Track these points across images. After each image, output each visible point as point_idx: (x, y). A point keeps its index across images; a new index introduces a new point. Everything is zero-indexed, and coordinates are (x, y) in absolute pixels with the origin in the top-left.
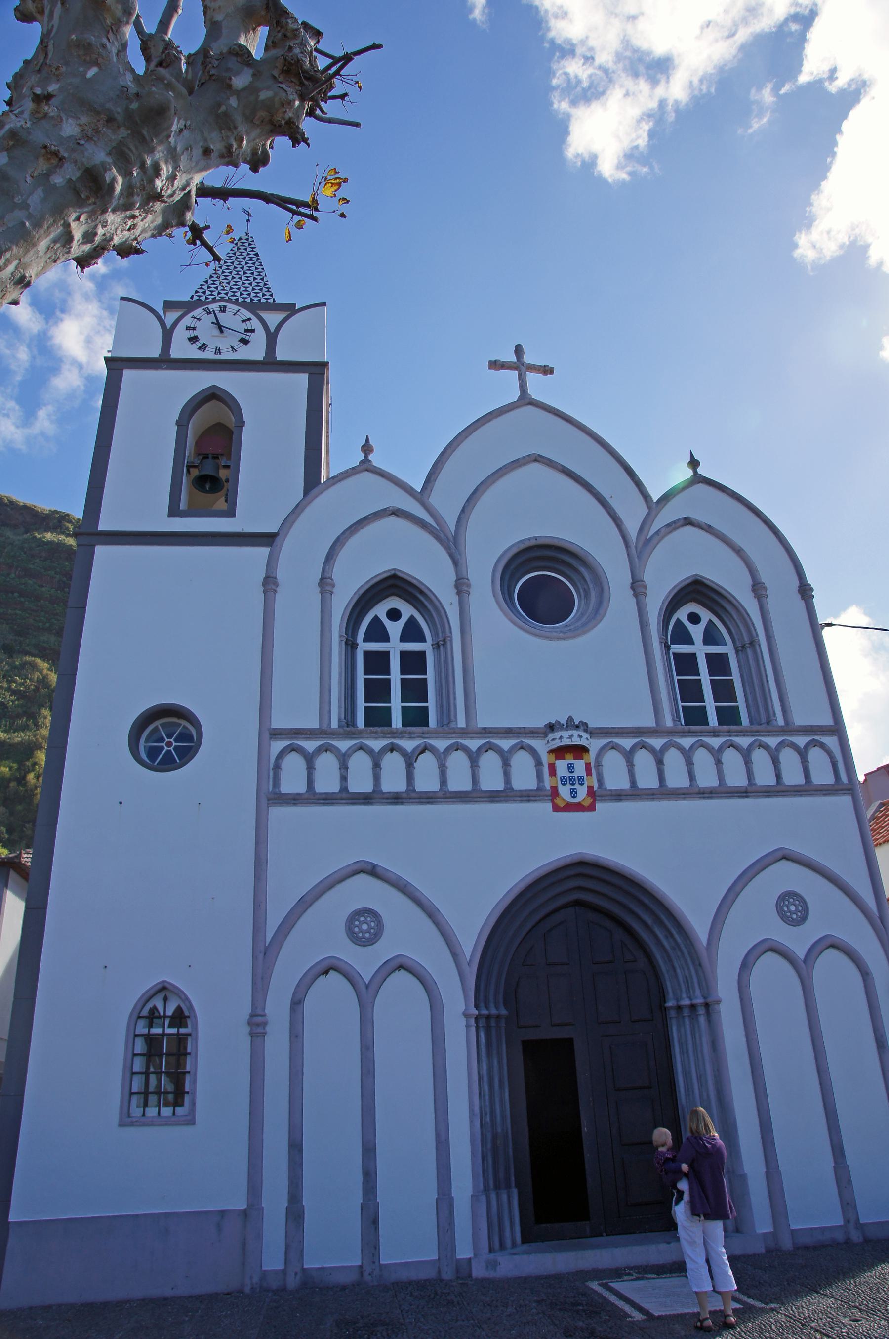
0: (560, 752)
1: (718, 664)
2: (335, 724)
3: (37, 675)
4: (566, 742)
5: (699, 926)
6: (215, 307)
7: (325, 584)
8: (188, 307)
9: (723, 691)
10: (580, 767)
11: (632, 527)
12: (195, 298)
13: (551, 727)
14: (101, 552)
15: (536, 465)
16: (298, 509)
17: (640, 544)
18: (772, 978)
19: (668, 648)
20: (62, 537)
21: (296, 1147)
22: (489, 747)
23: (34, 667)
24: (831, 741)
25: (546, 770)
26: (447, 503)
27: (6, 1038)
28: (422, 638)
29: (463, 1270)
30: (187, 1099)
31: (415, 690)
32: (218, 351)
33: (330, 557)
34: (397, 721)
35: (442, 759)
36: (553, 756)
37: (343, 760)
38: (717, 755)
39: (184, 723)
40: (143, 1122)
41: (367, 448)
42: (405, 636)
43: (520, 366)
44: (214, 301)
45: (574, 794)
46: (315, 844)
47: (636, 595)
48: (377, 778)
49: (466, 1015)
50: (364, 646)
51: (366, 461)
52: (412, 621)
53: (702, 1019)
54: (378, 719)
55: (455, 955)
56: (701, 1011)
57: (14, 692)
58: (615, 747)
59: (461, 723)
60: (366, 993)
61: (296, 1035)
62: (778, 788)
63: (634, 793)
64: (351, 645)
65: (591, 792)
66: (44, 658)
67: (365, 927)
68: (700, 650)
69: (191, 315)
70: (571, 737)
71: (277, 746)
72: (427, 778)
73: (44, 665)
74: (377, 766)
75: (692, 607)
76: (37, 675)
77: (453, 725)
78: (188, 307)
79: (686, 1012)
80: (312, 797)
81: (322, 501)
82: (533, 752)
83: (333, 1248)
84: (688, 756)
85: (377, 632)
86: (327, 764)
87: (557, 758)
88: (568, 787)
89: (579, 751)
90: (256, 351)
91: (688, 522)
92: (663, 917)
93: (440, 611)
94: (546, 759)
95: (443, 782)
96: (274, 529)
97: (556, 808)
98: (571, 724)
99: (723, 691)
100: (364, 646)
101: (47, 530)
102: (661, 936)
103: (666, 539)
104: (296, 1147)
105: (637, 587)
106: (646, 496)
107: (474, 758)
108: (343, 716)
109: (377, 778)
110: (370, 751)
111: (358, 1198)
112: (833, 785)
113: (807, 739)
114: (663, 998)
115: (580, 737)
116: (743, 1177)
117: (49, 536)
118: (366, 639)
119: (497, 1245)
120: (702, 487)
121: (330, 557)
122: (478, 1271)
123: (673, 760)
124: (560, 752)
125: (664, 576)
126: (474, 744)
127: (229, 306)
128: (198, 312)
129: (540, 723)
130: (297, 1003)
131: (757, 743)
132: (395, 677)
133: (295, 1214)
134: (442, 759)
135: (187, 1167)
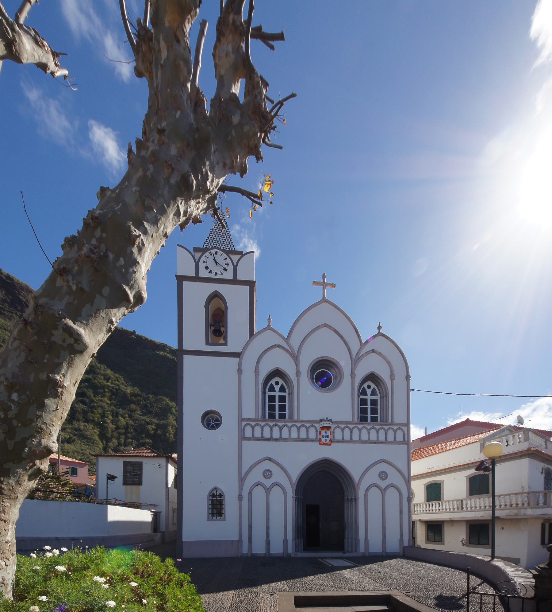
0: (323, 428)
1: (374, 402)
2: (260, 417)
3: (165, 402)
4: (326, 425)
5: (356, 476)
6: (213, 251)
7: (257, 371)
8: (203, 250)
9: (374, 411)
10: (328, 432)
11: (354, 353)
12: (205, 246)
13: (321, 421)
14: (186, 358)
16: (247, 344)
18: (375, 493)
19: (359, 396)
20: (165, 353)
21: (250, 527)
22: (303, 426)
23: (164, 400)
24: (405, 428)
27: (176, 502)
29: (289, 556)
30: (223, 515)
31: (282, 408)
32: (216, 274)
33: (258, 362)
39: (216, 416)
40: (213, 520)
41: (379, 327)
43: (324, 284)
44: (212, 248)
45: (326, 440)
46: (254, 451)
47: (352, 378)
48: (271, 434)
49: (293, 497)
51: (269, 325)
52: (282, 386)
53: (354, 502)
54: (272, 416)
56: (354, 500)
57: (159, 408)
59: (296, 418)
60: (268, 491)
61: (250, 501)
63: (343, 441)
64: (264, 393)
65: (331, 440)
66: (167, 397)
68: (369, 397)
69: (204, 255)
71: (244, 423)
73: (167, 399)
74: (271, 430)
75: (369, 383)
76: (165, 402)
78: (203, 250)
79: (350, 500)
80: (253, 438)
81: (257, 340)
82: (315, 428)
83: (259, 548)
84: (360, 430)
85: (272, 389)
86: (258, 430)
89: (328, 428)
90: (229, 275)
91: (373, 351)
93: (291, 382)
94: (319, 430)
96: (239, 351)
97: (320, 444)
98: (327, 420)
99: (374, 411)
100: (269, 393)
101: (160, 350)
104: (250, 527)
105: (353, 375)
106: (361, 341)
110: (270, 426)
111: (265, 538)
113: (362, 426)
114: (344, 497)
116: (359, 540)
117: (161, 353)
119: (297, 549)
120: (380, 337)
121: (258, 362)
122: (293, 555)
123: (356, 432)
124: (323, 428)
125: (362, 372)
126: (299, 425)
127: (219, 251)
128: (207, 254)
129: (318, 419)
130: (250, 493)
132: (277, 403)
133: (250, 541)
135: (225, 530)
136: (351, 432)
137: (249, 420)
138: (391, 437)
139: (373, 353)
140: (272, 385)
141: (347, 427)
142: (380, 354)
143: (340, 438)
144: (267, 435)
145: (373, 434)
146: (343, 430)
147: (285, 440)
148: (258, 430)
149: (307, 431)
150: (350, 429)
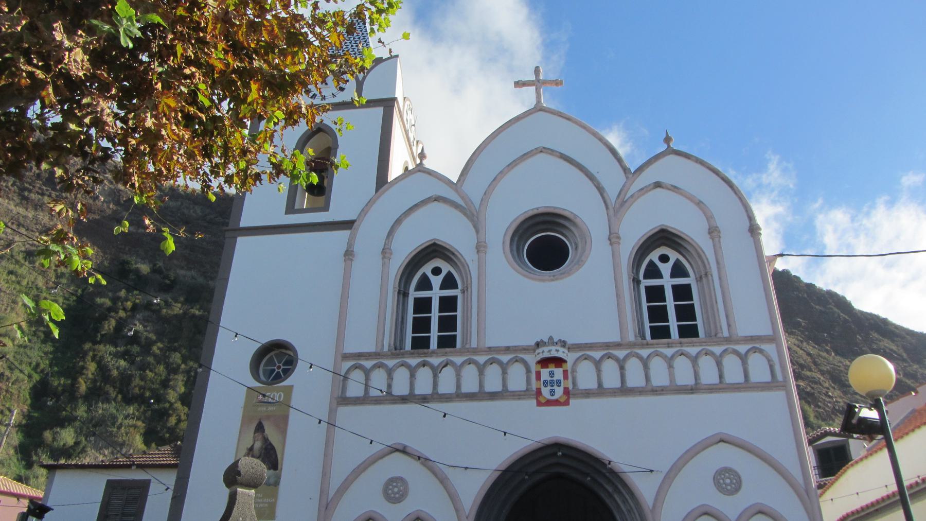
0: (545, 362)
2: (386, 349)
4: (546, 355)
7: (386, 252)
10: (558, 373)
11: (612, 193)
15: (542, 156)
16: (370, 203)
17: (617, 206)
22: (492, 361)
25: (533, 376)
26: (474, 191)
28: (686, 275)
31: (448, 324)
33: (391, 234)
34: (434, 343)
35: (458, 369)
36: (539, 366)
37: (390, 373)
38: (670, 361)
41: (668, 140)
42: (444, 286)
45: (552, 392)
50: (413, 294)
52: (449, 274)
54: (421, 344)
55: (457, 510)
58: (587, 358)
62: (721, 386)
63: (601, 391)
64: (636, 282)
65: (566, 391)
67: (396, 490)
70: (550, 351)
71: (348, 364)
72: (447, 384)
77: (719, 335)
81: (388, 195)
82: (525, 363)
85: (425, 284)
87: (542, 367)
88: (549, 388)
89: (558, 362)
91: (658, 185)
92: (620, 487)
94: (534, 368)
95: (458, 386)
97: (539, 404)
102: (620, 502)
103: (639, 200)
105: (613, 238)
107: (481, 369)
108: (392, 343)
109: (435, 384)
112: (768, 383)
113: (723, 348)
115: (557, 351)
118: (645, 277)
120: (672, 158)
121: (391, 234)
124: (545, 362)
125: (635, 229)
126: (482, 359)
131: (704, 352)
134: (458, 369)
136: (622, 368)
137: (360, 356)
138: (734, 373)
139: (659, 190)
140: (651, 263)
141: (609, 356)
142: (675, 189)
143: (593, 385)
144: (401, 387)
145: (658, 369)
146: (598, 364)
147: (493, 396)
148: (379, 379)
149: (504, 373)
150: (617, 359)
